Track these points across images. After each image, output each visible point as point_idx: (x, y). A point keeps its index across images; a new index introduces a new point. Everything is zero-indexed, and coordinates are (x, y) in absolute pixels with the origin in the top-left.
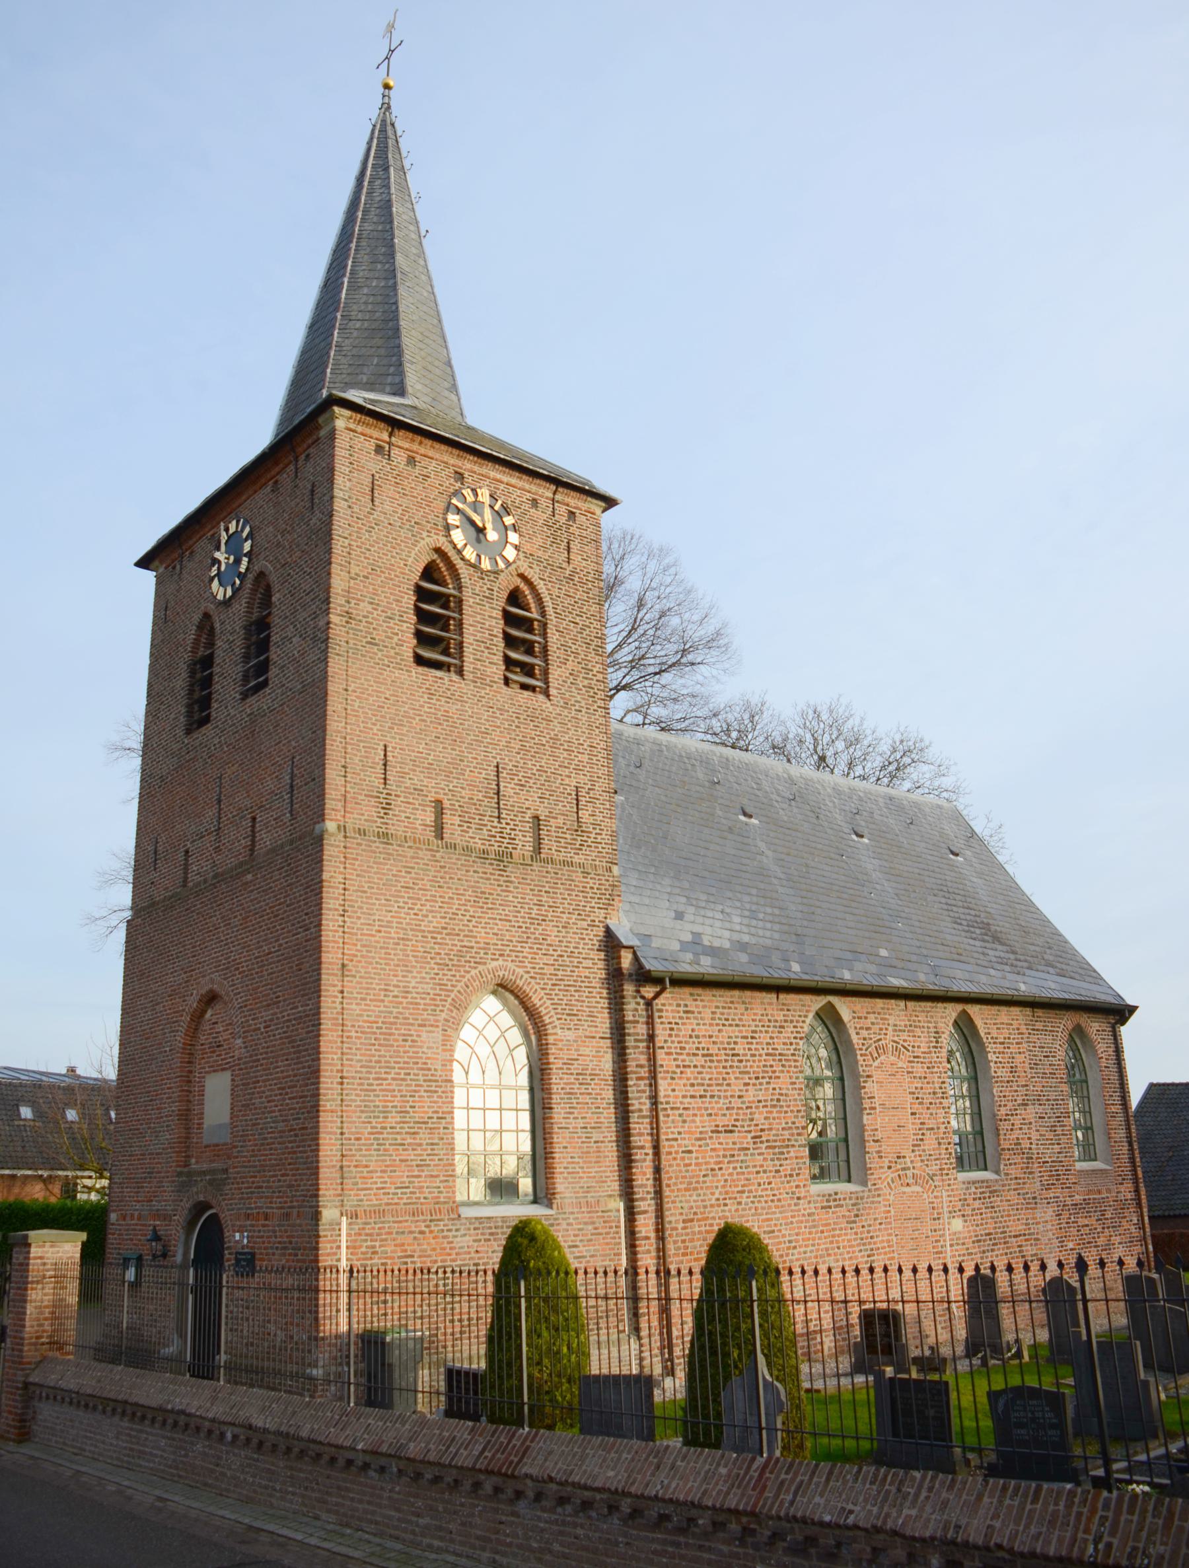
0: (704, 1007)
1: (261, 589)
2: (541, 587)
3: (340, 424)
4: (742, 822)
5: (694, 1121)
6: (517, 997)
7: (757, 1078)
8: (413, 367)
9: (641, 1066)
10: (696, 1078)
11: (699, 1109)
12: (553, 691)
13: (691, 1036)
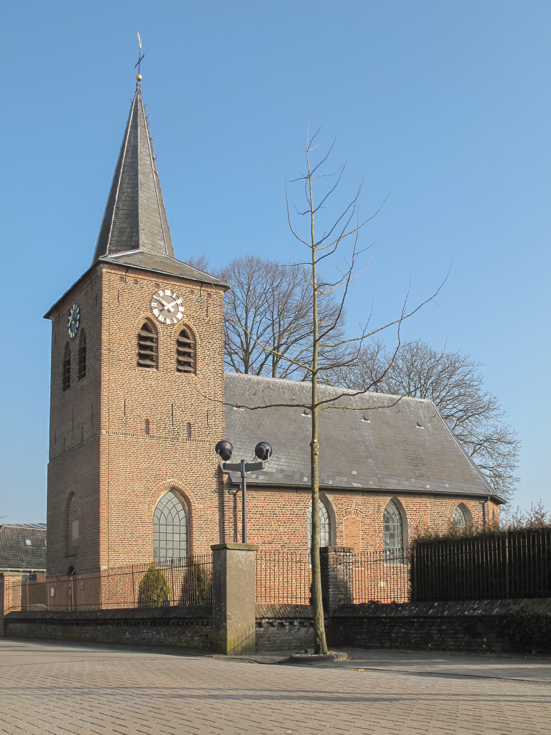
0: (261, 495)
1: (82, 335)
2: (194, 329)
3: (104, 270)
4: (304, 417)
5: (254, 539)
6: (180, 492)
7: (285, 523)
8: (143, 232)
9: (231, 518)
10: (255, 523)
11: (257, 534)
12: (198, 372)
13: (254, 507)
